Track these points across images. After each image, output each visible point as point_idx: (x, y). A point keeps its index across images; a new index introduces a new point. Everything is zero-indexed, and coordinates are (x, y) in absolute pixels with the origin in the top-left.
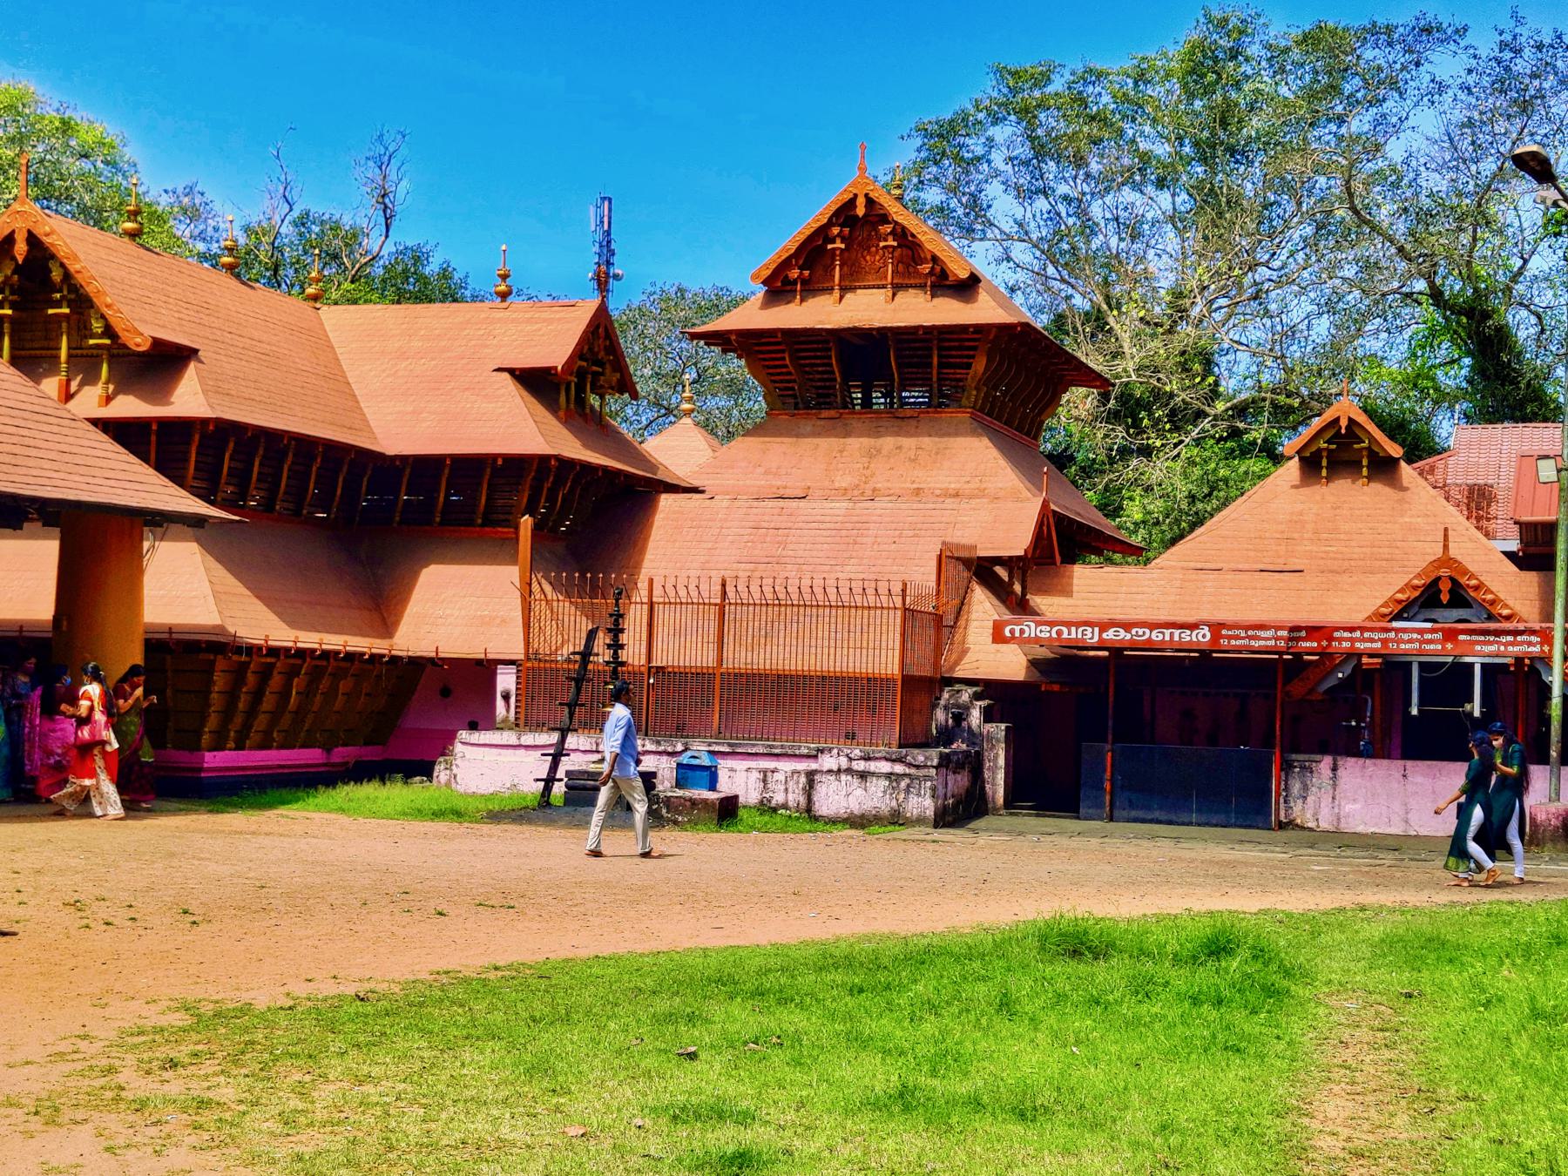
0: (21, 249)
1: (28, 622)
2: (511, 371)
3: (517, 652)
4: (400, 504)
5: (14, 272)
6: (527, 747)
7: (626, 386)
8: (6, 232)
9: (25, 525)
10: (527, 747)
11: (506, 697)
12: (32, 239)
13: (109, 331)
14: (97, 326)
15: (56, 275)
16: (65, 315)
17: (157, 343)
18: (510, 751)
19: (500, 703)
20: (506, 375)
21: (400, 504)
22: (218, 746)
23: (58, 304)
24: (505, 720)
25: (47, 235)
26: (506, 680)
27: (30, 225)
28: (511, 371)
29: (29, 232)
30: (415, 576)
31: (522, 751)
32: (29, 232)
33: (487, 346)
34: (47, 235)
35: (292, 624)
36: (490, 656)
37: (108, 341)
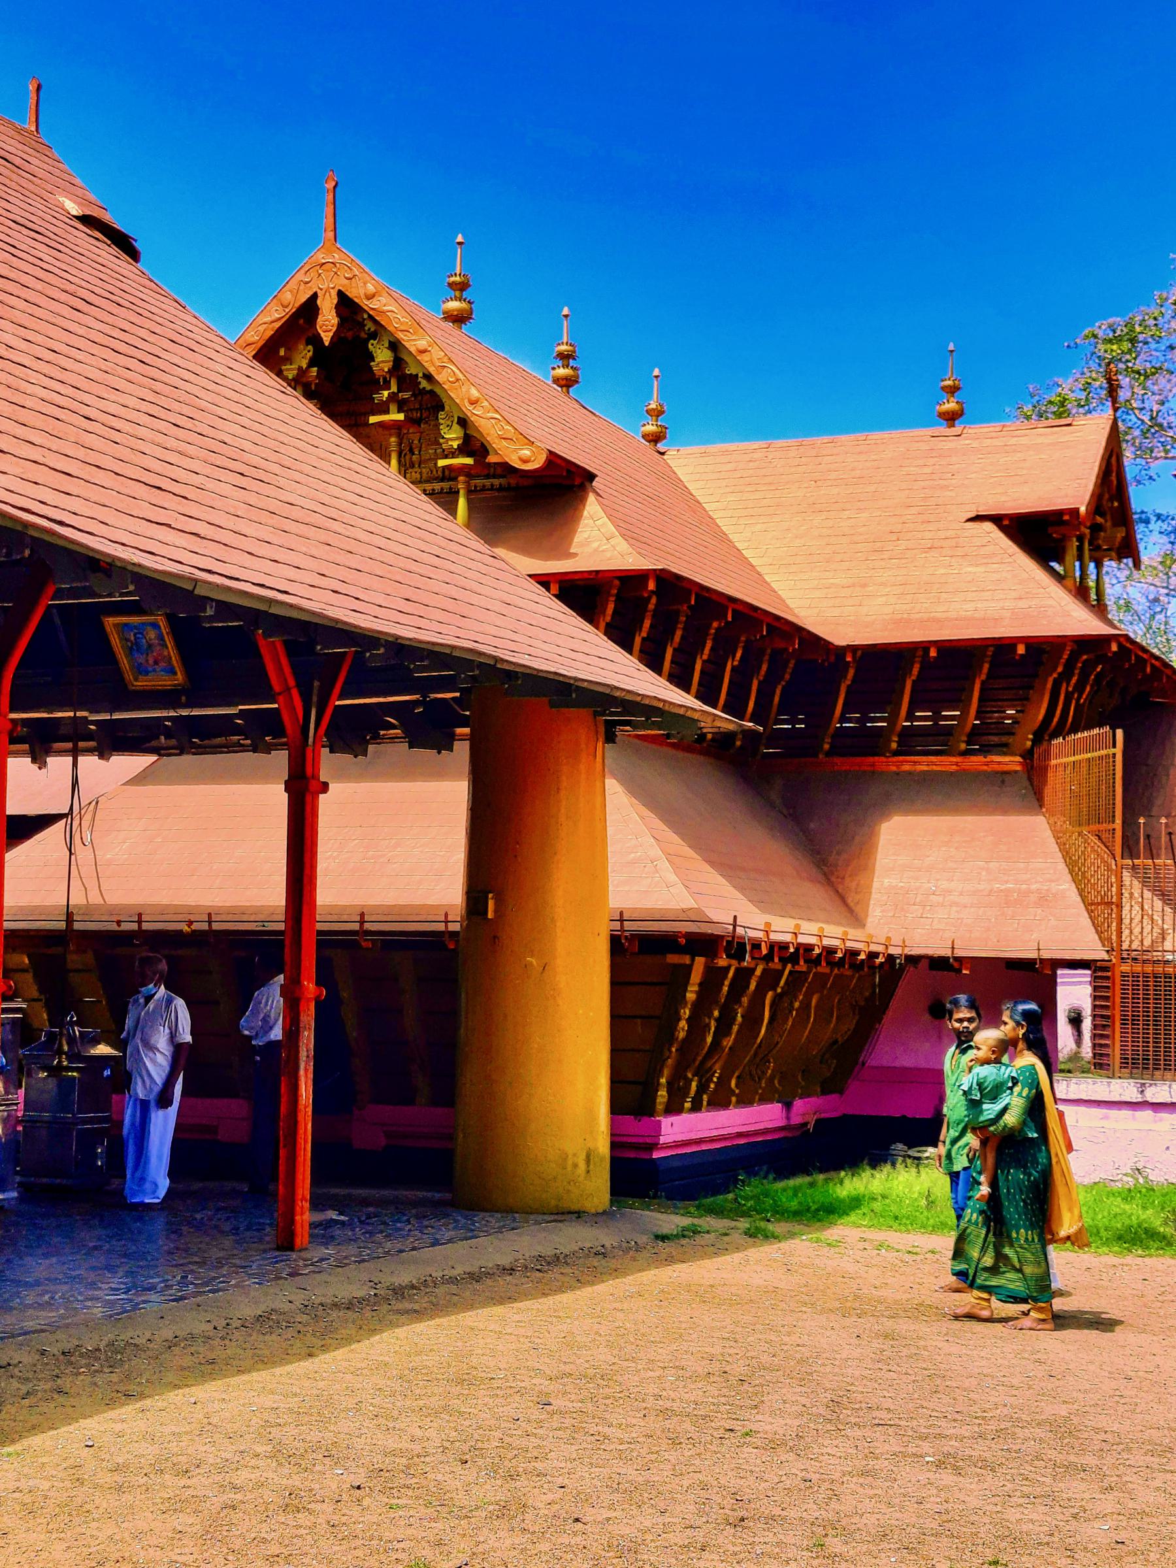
0: (328, 322)
1: (219, 910)
2: (996, 519)
3: (1091, 947)
4: (831, 730)
5: (312, 363)
6: (1158, 1107)
7: (1128, 550)
8: (303, 298)
9: (371, 748)
10: (1158, 1107)
11: (1076, 1021)
12: (346, 305)
13: (473, 445)
14: (452, 436)
15: (382, 357)
16: (396, 425)
17: (554, 460)
18: (1125, 1113)
19: (1064, 1030)
20: (989, 526)
21: (831, 730)
22: (674, 1108)
23: (383, 409)
24: (1075, 1057)
25: (370, 297)
26: (1074, 992)
27: (341, 283)
28: (996, 519)
29: (340, 294)
30: (872, 835)
31: (1148, 1114)
32: (340, 294)
33: (945, 488)
34: (370, 297)
35: (762, 902)
36: (1046, 955)
37: (469, 461)
